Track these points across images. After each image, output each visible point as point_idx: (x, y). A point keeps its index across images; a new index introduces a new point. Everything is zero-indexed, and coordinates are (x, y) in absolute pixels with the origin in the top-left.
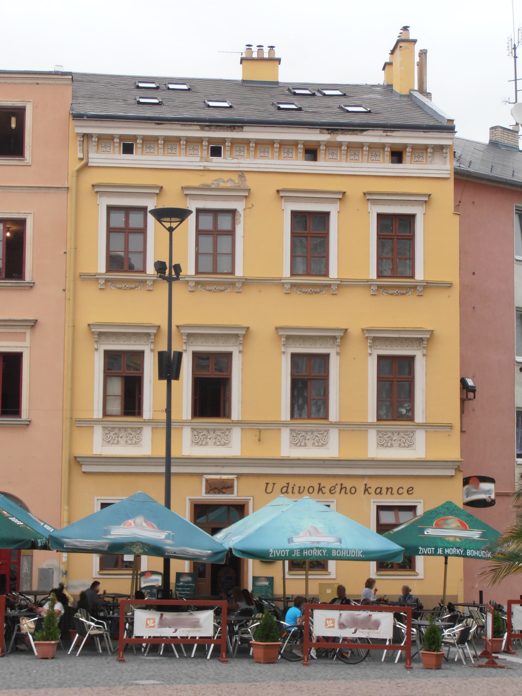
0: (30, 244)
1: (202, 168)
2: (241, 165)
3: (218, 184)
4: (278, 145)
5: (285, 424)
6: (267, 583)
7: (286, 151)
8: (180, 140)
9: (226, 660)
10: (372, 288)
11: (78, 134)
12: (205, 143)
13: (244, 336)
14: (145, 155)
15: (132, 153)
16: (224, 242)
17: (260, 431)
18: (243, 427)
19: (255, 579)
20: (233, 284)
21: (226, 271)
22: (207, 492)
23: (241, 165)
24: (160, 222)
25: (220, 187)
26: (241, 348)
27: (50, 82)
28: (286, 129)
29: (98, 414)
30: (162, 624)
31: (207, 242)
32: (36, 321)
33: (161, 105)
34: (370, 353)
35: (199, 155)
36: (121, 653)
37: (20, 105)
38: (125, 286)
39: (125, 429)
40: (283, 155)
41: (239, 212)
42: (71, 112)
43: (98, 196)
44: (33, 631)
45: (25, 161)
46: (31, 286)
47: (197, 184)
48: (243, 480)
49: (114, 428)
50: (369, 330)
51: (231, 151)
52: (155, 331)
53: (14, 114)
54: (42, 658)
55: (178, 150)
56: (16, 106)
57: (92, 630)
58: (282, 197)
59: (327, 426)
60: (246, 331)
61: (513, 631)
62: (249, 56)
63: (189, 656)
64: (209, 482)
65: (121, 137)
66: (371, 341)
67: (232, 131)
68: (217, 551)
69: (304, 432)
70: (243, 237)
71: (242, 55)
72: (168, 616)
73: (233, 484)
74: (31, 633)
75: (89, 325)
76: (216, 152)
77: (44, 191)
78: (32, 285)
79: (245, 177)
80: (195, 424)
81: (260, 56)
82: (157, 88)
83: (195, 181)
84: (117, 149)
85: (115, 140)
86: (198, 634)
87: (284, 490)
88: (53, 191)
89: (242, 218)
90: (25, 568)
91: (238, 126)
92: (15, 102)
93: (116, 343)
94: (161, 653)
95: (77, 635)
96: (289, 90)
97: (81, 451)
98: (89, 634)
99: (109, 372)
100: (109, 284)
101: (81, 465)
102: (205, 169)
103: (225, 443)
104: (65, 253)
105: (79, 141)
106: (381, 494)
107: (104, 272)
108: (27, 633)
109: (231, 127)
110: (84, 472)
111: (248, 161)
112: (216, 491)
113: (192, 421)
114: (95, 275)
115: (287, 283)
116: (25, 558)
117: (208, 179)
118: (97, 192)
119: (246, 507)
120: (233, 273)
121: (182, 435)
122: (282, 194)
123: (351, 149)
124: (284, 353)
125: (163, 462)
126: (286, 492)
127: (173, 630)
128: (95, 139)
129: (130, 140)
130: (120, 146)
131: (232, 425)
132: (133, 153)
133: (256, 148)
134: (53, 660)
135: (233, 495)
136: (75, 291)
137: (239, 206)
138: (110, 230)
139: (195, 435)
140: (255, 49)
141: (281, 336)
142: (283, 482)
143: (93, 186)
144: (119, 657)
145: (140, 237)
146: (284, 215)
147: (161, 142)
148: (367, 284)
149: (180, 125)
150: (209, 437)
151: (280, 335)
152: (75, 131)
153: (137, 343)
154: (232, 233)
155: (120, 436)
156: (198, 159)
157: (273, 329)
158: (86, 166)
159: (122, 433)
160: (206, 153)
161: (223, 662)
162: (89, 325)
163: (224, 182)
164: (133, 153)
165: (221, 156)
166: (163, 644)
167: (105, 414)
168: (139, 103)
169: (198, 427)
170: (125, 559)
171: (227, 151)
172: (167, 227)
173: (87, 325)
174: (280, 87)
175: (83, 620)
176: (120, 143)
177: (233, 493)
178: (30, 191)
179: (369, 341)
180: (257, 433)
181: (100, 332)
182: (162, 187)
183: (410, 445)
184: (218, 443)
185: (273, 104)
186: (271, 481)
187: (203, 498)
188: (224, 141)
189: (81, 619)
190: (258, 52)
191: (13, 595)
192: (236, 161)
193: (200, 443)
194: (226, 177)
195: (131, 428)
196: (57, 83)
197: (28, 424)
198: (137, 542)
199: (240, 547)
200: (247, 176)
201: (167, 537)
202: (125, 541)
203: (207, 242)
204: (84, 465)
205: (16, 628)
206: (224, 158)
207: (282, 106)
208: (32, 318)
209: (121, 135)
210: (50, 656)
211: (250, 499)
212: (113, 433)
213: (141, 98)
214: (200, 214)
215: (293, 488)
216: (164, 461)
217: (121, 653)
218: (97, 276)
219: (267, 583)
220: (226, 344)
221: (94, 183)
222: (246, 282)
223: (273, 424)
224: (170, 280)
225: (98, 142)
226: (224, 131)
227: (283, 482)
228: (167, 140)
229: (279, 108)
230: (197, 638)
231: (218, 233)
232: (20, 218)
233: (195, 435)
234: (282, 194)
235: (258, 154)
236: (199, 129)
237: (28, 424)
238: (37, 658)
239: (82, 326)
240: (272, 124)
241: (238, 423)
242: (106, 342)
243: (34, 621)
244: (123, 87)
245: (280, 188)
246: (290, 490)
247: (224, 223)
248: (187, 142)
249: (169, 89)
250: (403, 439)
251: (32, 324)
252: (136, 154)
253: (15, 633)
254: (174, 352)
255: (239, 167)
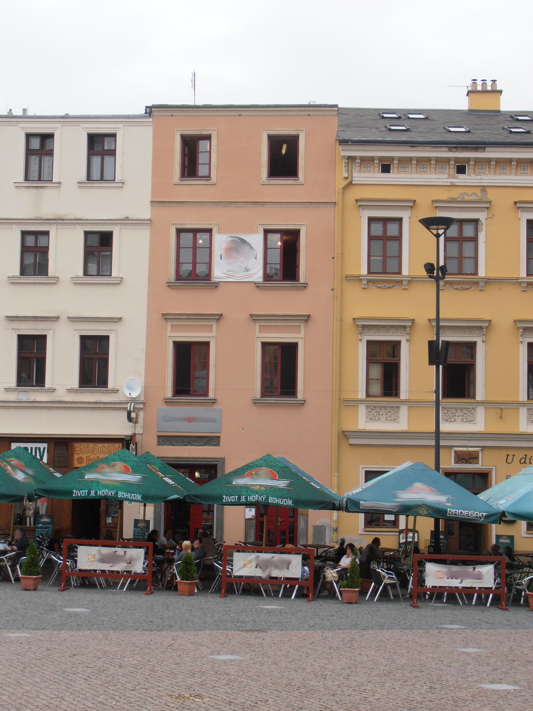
0: (304, 251)
1: (449, 184)
2: (483, 181)
3: (463, 197)
4: (516, 163)
5: (523, 404)
6: (508, 541)
7: (480, 167)
8: (431, 160)
9: (506, 608)
10: (522, 285)
11: (344, 157)
12: (452, 163)
13: (411, 327)
14: (400, 173)
15: (389, 172)
16: (392, 246)
17: (502, 410)
18: (487, 406)
19: (498, 537)
20: (476, 283)
21: (469, 273)
22: (456, 462)
23: (483, 181)
24: (429, 229)
25: (466, 200)
26: (484, 338)
27: (319, 113)
28: (523, 149)
29: (362, 395)
30: (452, 576)
31: (378, 245)
32: (309, 316)
33: (409, 131)
34: (521, 341)
35: (447, 173)
36: (415, 600)
37: (294, 133)
38: (384, 286)
39: (385, 408)
40: (478, 171)
41: (481, 221)
42: (338, 138)
43: (520, 212)
44: (337, 579)
45: (299, 181)
46: (305, 286)
47: (445, 198)
48: (487, 452)
49: (376, 407)
50: (520, 321)
51: (474, 168)
52: (410, 324)
53: (285, 142)
54: (347, 603)
55: (428, 169)
56: (291, 135)
57: (387, 579)
58: (519, 208)
59: (475, 404)
60: (489, 324)
61: (498, 584)
62: (474, 89)
63: (470, 604)
64: (458, 453)
65: (381, 159)
66: (522, 331)
67: (475, 151)
68: (490, 514)
69: (453, 410)
70: (485, 242)
71: (468, 88)
72: (455, 568)
73: (479, 455)
74: (335, 581)
75: (354, 319)
76: (461, 170)
77: (175, 205)
78: (305, 285)
79: (486, 191)
80: (445, 404)
81: (484, 89)
82: (399, 118)
83: (443, 195)
84: (376, 169)
85: (375, 161)
86: (477, 584)
87: (523, 461)
88: (323, 206)
89: (484, 227)
90: (301, 524)
91: (481, 147)
92: (290, 131)
93: (377, 334)
94: (444, 601)
95: (373, 584)
96: (511, 117)
97: (348, 427)
98: (385, 583)
99: (371, 360)
100: (371, 284)
101: (349, 438)
102: (452, 184)
103: (471, 420)
104: (333, 258)
105: (345, 163)
106: (525, 463)
107: (366, 274)
108: (332, 581)
109: (474, 148)
110: (350, 444)
111: (489, 177)
112: (464, 461)
113: (367, 399)
114: (359, 277)
115: (524, 282)
116: (301, 516)
117: (455, 193)
118: (360, 206)
119: (489, 475)
120: (476, 273)
121: (519, 413)
122: (518, 205)
123: (500, 164)
124: (521, 342)
125: (432, 437)
126: (524, 462)
127: (459, 580)
128: (358, 161)
129: (387, 161)
130: (379, 167)
131: (477, 404)
132: (390, 173)
133: (496, 165)
134: (356, 605)
135: (478, 465)
136: (342, 291)
137: (481, 216)
138: (371, 238)
139: (445, 413)
140: (479, 83)
141: (518, 328)
142: (521, 454)
143: (356, 200)
144: (414, 603)
145: (396, 243)
146: (362, 221)
147: (414, 162)
148: (516, 282)
149: (431, 148)
150: (457, 415)
151: (518, 327)
152: (340, 154)
153: (395, 334)
154: (475, 240)
155: (381, 413)
156: (446, 176)
157: (512, 322)
158: (350, 184)
159: (383, 411)
160: (453, 171)
161: (504, 609)
162: (354, 319)
163: (468, 195)
164: (390, 173)
165: (465, 173)
166: (446, 593)
167: (368, 395)
168: (390, 130)
169: (448, 406)
170: (385, 519)
171: (414, 168)
172: (435, 234)
173: (352, 319)
174: (503, 114)
175: (380, 571)
176: (379, 164)
177: (478, 463)
178: (303, 206)
179: (520, 330)
180: (499, 411)
181: (363, 325)
182: (415, 201)
183: (395, 420)
184: (465, 420)
185: (503, 128)
186: (511, 453)
187: (452, 467)
188: (468, 160)
189: (377, 570)
190: (482, 85)
191: (298, 547)
192: (479, 177)
193: (449, 420)
194: (470, 191)
195: (390, 407)
196: (326, 114)
197: (303, 403)
198: (423, 504)
199: (511, 510)
200: (488, 190)
201: (448, 501)
202: (412, 504)
203: (378, 245)
204: (351, 438)
205: (322, 577)
206: (468, 175)
207: (513, 130)
208: (306, 314)
209: (518, 158)
210: (354, 601)
211: (493, 469)
212: (375, 411)
213: (390, 126)
214: (372, 222)
215: (530, 459)
216: (434, 435)
217: (415, 600)
218: (360, 278)
219: (508, 541)
220: (471, 335)
221: (357, 198)
222: (488, 281)
223: (512, 403)
224: (437, 279)
225: (361, 163)
226: (468, 152)
227: (521, 454)
228: (420, 160)
229: (511, 132)
230: (477, 589)
231: (464, 239)
232: (295, 229)
233: (445, 413)
234: (518, 205)
235: (498, 171)
236: (447, 150)
237: (303, 403)
238: (343, 602)
239: (348, 320)
240: (511, 145)
241: (482, 403)
242: (368, 334)
243: (337, 572)
244: (370, 117)
245: (517, 200)
246: (528, 461)
247: (468, 231)
248: (518, 163)
249: (409, 118)
250: (466, 415)
251: (306, 318)
252: (393, 173)
253: (321, 581)
254: (442, 341)
255: (482, 182)
